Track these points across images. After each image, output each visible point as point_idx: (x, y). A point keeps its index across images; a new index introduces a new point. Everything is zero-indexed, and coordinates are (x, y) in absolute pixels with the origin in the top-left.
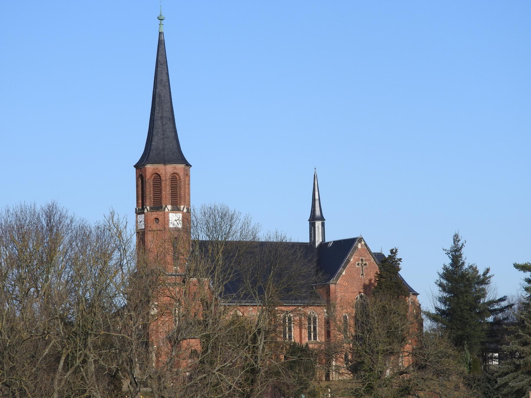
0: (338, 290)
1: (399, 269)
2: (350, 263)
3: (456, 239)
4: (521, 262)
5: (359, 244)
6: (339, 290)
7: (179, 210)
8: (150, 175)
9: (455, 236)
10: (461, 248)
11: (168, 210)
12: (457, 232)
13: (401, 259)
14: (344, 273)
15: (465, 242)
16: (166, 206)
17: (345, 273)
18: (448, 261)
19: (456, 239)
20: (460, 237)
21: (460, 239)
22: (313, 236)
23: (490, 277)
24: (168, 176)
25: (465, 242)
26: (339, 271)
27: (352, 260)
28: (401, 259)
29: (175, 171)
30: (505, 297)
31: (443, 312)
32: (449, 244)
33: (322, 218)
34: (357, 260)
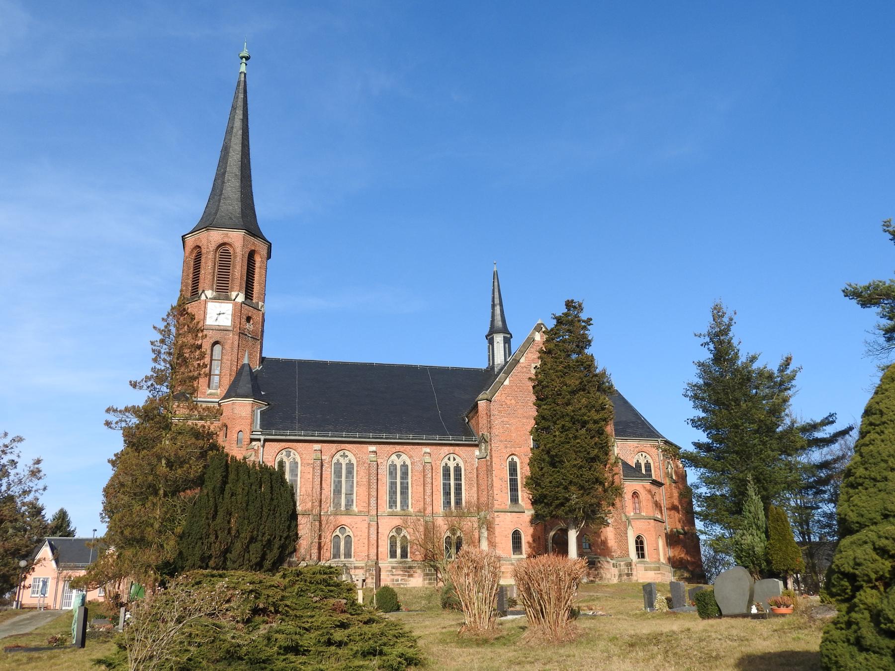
0: (494, 412)
1: (589, 343)
2: (519, 365)
3: (718, 313)
4: (862, 281)
5: (537, 333)
6: (496, 413)
7: (227, 298)
8: (190, 250)
9: (715, 309)
10: (729, 325)
11: (207, 297)
12: (718, 301)
13: (591, 319)
14: (507, 382)
15: (735, 313)
16: (203, 291)
17: (510, 383)
18: (706, 356)
19: (718, 313)
20: (724, 306)
21: (725, 311)
22: (491, 358)
23: (795, 372)
24: (213, 247)
25: (735, 313)
26: (497, 379)
27: (522, 360)
28: (591, 319)
29: (226, 240)
30: (831, 415)
31: (707, 448)
32: (705, 324)
33: (505, 330)
34: (533, 360)
